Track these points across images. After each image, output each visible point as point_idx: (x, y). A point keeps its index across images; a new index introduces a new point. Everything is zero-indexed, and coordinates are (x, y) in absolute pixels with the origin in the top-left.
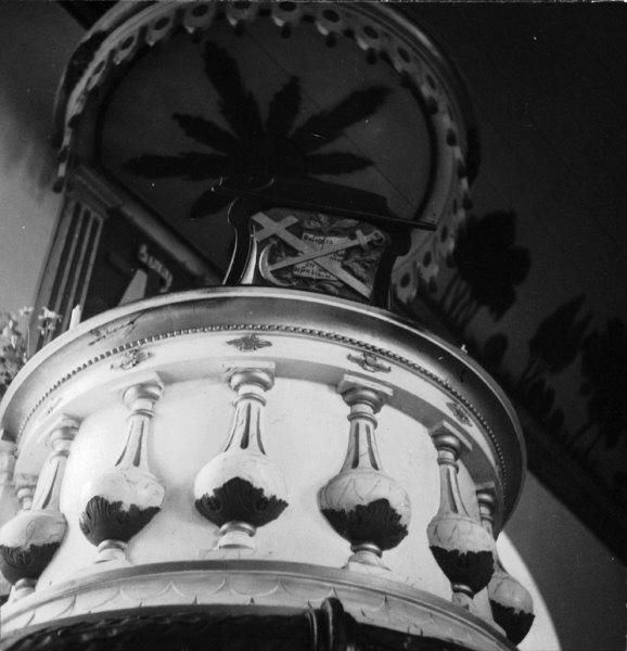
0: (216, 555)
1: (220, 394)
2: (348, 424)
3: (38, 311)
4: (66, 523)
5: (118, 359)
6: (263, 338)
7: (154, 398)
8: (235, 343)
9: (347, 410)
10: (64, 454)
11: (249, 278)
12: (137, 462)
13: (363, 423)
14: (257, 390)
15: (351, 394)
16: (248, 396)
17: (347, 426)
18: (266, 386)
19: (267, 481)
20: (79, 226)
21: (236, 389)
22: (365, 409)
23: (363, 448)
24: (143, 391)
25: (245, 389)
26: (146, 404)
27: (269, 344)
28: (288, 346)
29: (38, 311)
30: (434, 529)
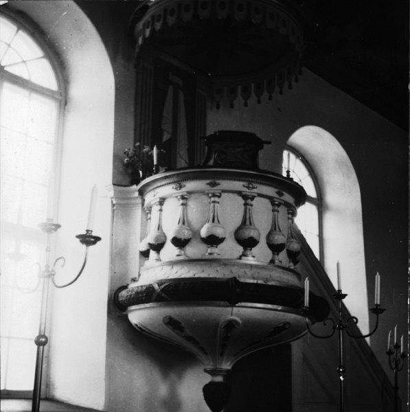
0: (207, 256)
1: (205, 199)
2: (243, 207)
3: (140, 148)
4: (165, 236)
5: (174, 186)
6: (218, 181)
7: (186, 199)
8: (208, 184)
9: (243, 202)
10: (161, 210)
11: (211, 162)
12: (184, 223)
13: (249, 207)
14: (217, 199)
15: (245, 197)
16: (214, 202)
17: (243, 207)
18: (219, 197)
19: (219, 232)
20: (142, 136)
21: (210, 197)
22: (249, 201)
23: (248, 216)
24: (183, 198)
25: (213, 199)
26: (184, 201)
27: (219, 184)
28: (225, 184)
29: (135, 143)
30: (268, 237)
